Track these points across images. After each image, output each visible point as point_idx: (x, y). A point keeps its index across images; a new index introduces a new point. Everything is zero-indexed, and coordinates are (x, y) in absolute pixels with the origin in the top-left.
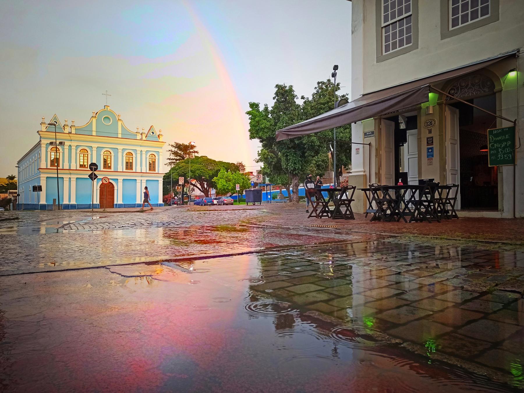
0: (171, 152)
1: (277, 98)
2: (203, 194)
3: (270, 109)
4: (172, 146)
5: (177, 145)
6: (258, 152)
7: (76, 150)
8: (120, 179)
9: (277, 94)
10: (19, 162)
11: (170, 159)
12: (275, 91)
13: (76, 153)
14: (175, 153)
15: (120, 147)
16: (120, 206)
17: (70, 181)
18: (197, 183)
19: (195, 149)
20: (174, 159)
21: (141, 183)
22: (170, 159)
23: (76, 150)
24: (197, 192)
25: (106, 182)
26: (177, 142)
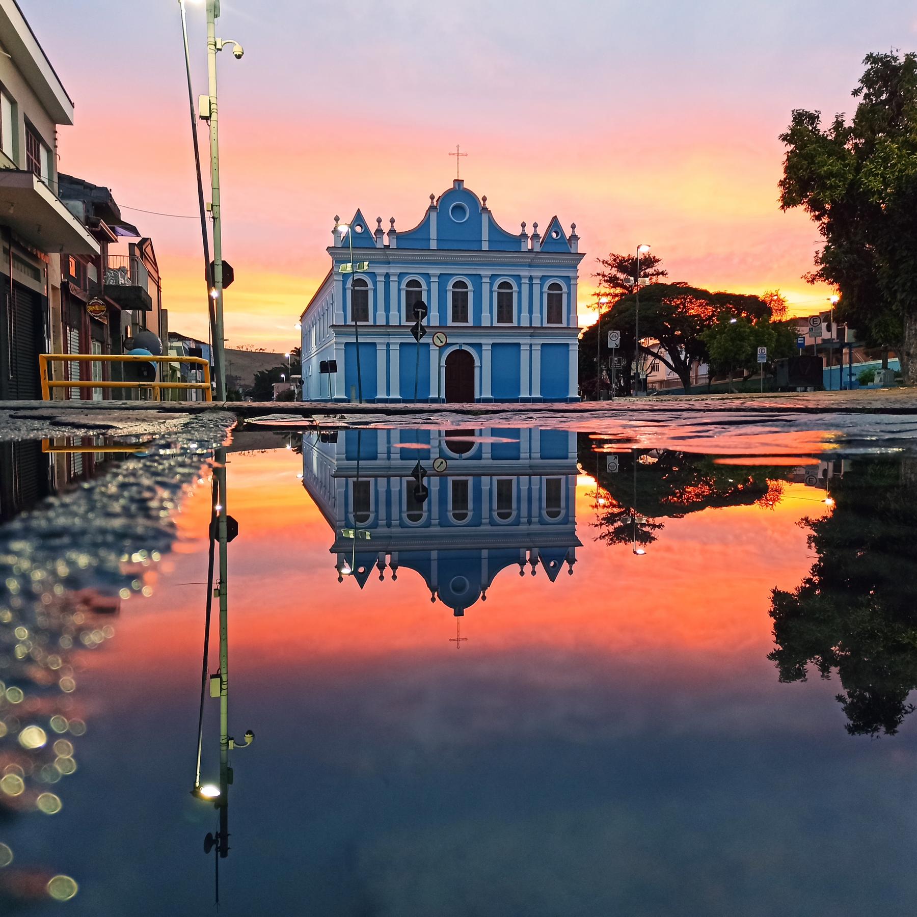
0: (601, 277)
1: (865, 90)
2: (677, 376)
3: (849, 123)
4: (604, 262)
5: (615, 260)
6: (817, 253)
7: (399, 283)
8: (487, 342)
9: (867, 80)
10: (302, 317)
12: (861, 74)
14: (613, 281)
15: (486, 272)
17: (388, 351)
18: (663, 350)
19: (659, 267)
21: (531, 351)
24: (663, 373)
25: (442, 342)
26: (616, 254)
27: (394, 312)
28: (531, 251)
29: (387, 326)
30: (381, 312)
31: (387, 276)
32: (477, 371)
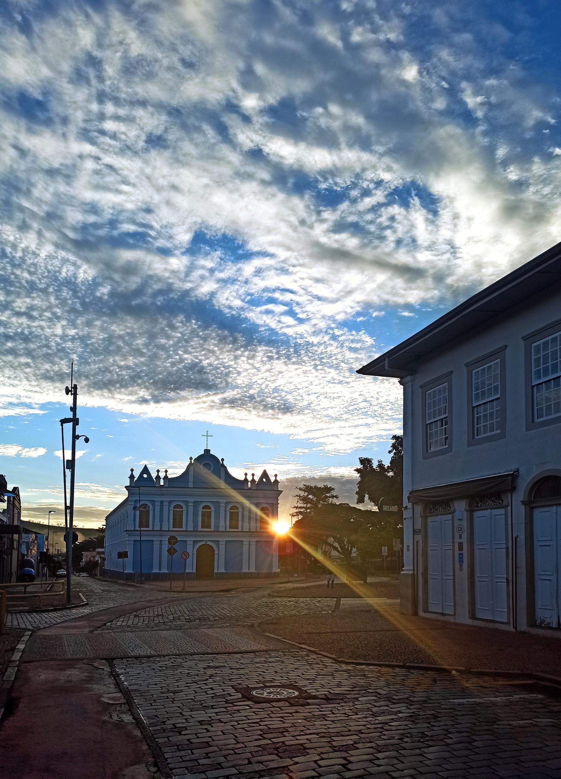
1: (394, 451)
4: (300, 489)
5: (306, 488)
7: (169, 506)
11: (297, 508)
13: (169, 510)
14: (304, 499)
16: (221, 576)
17: (161, 545)
19: (334, 493)
20: (304, 507)
22: (297, 508)
23: (169, 506)
27: (165, 523)
28: (250, 489)
29: (161, 530)
30: (157, 522)
31: (162, 502)
32: (216, 556)
